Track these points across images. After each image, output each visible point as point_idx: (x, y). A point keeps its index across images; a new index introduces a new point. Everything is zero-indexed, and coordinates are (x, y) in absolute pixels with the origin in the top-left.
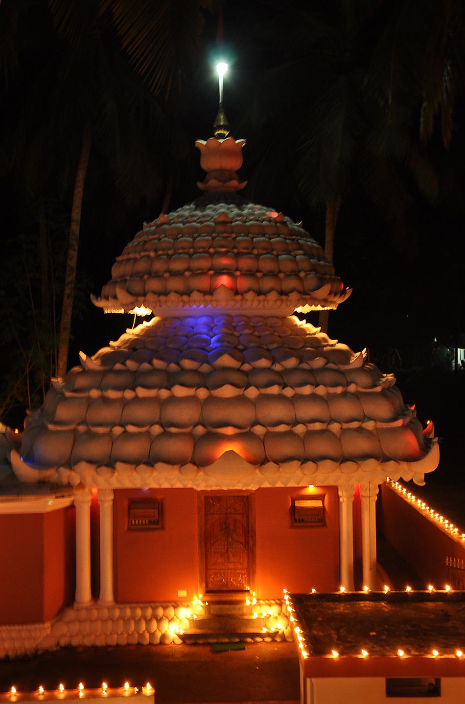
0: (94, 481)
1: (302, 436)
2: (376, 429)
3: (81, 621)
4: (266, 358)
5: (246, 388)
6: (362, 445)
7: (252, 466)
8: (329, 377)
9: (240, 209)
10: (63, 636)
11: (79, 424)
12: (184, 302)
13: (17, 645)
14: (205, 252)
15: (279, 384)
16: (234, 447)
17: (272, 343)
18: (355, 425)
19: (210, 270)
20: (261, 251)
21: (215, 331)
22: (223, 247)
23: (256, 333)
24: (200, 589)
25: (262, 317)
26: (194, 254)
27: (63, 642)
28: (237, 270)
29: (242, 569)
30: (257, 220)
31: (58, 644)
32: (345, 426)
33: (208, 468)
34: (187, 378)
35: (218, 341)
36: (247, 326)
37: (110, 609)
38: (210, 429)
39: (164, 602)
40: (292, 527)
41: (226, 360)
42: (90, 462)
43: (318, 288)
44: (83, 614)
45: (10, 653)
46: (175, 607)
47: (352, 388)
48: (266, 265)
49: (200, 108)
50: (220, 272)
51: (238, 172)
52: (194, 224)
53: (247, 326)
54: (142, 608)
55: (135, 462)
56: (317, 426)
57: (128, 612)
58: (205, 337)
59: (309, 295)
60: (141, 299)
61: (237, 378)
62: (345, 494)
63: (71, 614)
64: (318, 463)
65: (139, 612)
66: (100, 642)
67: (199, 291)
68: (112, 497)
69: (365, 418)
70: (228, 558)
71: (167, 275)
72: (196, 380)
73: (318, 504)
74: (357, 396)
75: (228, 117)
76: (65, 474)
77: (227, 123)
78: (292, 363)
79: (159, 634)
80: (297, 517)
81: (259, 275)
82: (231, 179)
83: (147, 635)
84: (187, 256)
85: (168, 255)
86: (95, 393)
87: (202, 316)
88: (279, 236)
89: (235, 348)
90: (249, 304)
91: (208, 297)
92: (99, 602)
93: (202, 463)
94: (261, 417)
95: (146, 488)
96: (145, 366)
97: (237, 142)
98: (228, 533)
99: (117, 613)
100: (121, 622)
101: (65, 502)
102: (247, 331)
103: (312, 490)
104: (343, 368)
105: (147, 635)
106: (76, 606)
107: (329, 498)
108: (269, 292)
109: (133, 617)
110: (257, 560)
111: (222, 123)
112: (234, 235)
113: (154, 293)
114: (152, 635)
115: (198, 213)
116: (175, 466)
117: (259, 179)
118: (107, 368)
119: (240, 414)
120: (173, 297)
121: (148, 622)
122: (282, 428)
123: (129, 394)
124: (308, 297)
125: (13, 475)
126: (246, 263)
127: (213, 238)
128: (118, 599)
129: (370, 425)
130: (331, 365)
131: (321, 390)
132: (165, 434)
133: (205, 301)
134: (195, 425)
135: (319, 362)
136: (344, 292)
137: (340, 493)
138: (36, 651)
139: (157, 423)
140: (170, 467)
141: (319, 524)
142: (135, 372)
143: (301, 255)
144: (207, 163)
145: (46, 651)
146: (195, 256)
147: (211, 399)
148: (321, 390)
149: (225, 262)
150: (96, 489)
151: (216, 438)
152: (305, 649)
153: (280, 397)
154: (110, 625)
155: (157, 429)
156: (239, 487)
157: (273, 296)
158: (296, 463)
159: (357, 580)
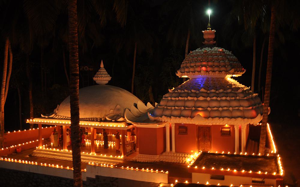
1: (221, 111)
4: (222, 89)
6: (238, 114)
7: (205, 119)
8: (231, 95)
12: (194, 74)
13: (150, 159)
14: (200, 61)
15: (216, 97)
16: (201, 114)
17: (218, 85)
18: (237, 108)
19: (201, 65)
20: (215, 60)
21: (203, 82)
22: (204, 59)
23: (214, 83)
24: (197, 151)
27: (161, 160)
28: (214, 65)
29: (208, 146)
30: (215, 52)
32: (234, 108)
33: (193, 119)
34: (192, 95)
35: (203, 85)
36: (212, 80)
37: (174, 153)
40: (221, 136)
41: (203, 90)
42: (166, 116)
43: (230, 70)
44: (172, 154)
47: (238, 98)
48: (216, 64)
49: (204, 22)
50: (203, 66)
51: (214, 39)
52: (198, 53)
53: (212, 80)
54: (182, 154)
55: (175, 116)
56: (225, 108)
57: (178, 155)
58: (200, 83)
60: (183, 74)
61: (204, 95)
63: (164, 154)
65: (181, 155)
66: (170, 161)
67: (197, 71)
68: (174, 125)
69: (240, 106)
70: (205, 143)
71: (190, 67)
72: (194, 95)
73: (229, 130)
74: (239, 100)
77: (211, 26)
78: (221, 91)
79: (184, 161)
81: (214, 67)
82: (211, 40)
86: (169, 98)
87: (201, 78)
90: (211, 75)
91: (199, 73)
92: (172, 152)
93: (192, 117)
94: (210, 105)
95: (183, 123)
96: (183, 91)
97: (212, 31)
101: (162, 126)
102: (211, 82)
103: (227, 126)
104: (236, 92)
105: (181, 161)
106: (166, 152)
109: (179, 156)
111: (209, 26)
112: (208, 56)
113: (186, 72)
114: (183, 161)
115: (200, 50)
116: (185, 118)
117: (219, 41)
118: (174, 92)
119: (204, 105)
121: (182, 158)
122: (215, 109)
123: (177, 99)
124: (227, 72)
125: (149, 119)
126: (210, 64)
127: (202, 57)
128: (177, 151)
129: (241, 108)
130: (233, 91)
131: (228, 98)
132: (185, 109)
133: (219, 73)
135: (229, 91)
136: (243, 71)
137: (235, 127)
139: (183, 106)
140: (184, 118)
141: (229, 135)
142: (180, 93)
144: (205, 37)
145: (156, 162)
147: (198, 100)
149: (204, 63)
151: (196, 110)
152: (282, 169)
155: (183, 108)
156: (207, 124)
157: (217, 72)
158: (217, 118)
159: (240, 150)
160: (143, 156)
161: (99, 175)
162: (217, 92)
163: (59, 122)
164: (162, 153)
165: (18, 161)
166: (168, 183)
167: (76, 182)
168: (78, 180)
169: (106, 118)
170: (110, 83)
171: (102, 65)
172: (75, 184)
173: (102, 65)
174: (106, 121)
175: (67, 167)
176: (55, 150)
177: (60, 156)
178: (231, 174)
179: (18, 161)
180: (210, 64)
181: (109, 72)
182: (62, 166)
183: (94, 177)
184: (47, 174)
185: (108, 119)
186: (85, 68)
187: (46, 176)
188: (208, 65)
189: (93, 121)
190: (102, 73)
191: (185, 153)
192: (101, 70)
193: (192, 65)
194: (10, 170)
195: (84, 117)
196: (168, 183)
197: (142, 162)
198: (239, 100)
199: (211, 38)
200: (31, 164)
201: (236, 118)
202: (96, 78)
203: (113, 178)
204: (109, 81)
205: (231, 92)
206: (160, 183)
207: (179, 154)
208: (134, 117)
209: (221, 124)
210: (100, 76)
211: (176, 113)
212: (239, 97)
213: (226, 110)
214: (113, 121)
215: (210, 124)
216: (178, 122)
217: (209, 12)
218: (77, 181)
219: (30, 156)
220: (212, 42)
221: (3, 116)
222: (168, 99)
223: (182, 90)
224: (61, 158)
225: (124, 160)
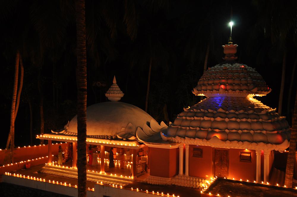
0: (184, 142)
2: (267, 133)
3: (179, 179)
5: (225, 118)
6: (260, 138)
7: (221, 141)
9: (232, 65)
10: (174, 182)
11: (179, 126)
13: (162, 182)
16: (218, 136)
18: (259, 131)
24: (212, 176)
25: (238, 97)
26: (235, 79)
27: (173, 184)
31: (172, 184)
32: (255, 132)
34: (209, 115)
38: (213, 130)
39: (202, 178)
41: (220, 110)
42: (179, 136)
44: (180, 177)
45: (160, 184)
46: (205, 180)
47: (260, 120)
48: (237, 82)
50: (222, 84)
55: (190, 137)
56: (246, 131)
59: (250, 91)
60: (200, 92)
61: (223, 115)
62: (258, 153)
63: (177, 177)
64: (244, 142)
65: (194, 179)
67: (215, 90)
68: (189, 147)
70: (221, 168)
73: (249, 155)
74: (262, 123)
75: (232, 38)
76: (173, 139)
79: (198, 186)
80: (241, 158)
83: (195, 186)
84: (213, 79)
85: (209, 79)
86: (184, 118)
88: (243, 73)
89: (234, 107)
91: (217, 91)
92: (185, 175)
93: (208, 139)
94: (228, 127)
99: (189, 178)
100: (192, 181)
103: (247, 150)
107: (252, 154)
108: (236, 90)
109: (192, 181)
111: (231, 40)
113: (203, 90)
117: (240, 57)
120: (208, 91)
121: (196, 182)
122: (234, 131)
123: (192, 118)
124: (249, 91)
126: (230, 81)
129: (264, 132)
130: (255, 113)
131: (249, 120)
132: (200, 130)
134: (209, 128)
135: (251, 112)
136: (268, 91)
137: (256, 153)
138: (166, 184)
139: (198, 127)
140: (199, 139)
142: (196, 112)
143: (249, 78)
144: (225, 52)
146: (215, 79)
148: (249, 120)
149: (223, 81)
150: (183, 144)
151: (213, 132)
153: (236, 122)
155: (198, 129)
157: (237, 91)
161: (107, 195)
164: (174, 176)
165: (27, 177)
169: (117, 137)
170: (123, 100)
171: (115, 81)
173: (115, 81)
174: (116, 139)
179: (64, 184)
185: (119, 137)
189: (104, 139)
190: (114, 89)
192: (114, 86)
193: (210, 82)
198: (262, 123)
204: (122, 98)
210: (112, 92)
211: (190, 134)
216: (193, 144)
224: (70, 176)
225: (134, 181)
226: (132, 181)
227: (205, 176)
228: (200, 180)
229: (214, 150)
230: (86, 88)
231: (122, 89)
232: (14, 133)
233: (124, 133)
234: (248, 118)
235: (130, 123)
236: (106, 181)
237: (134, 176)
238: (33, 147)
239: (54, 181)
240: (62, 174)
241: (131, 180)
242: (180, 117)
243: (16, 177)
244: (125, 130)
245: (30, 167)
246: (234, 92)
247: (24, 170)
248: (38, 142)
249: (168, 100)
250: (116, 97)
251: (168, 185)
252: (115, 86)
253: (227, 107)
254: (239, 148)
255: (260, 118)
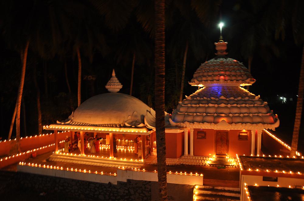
6: (258, 120)
8: (241, 102)
10: (181, 162)
11: (186, 113)
18: (256, 114)
32: (254, 115)
33: (217, 124)
34: (212, 102)
41: (222, 97)
45: (169, 164)
47: (256, 105)
48: (233, 73)
49: (216, 35)
56: (246, 114)
60: (201, 82)
61: (225, 102)
63: (183, 157)
65: (199, 158)
68: (193, 130)
70: (222, 147)
71: (207, 76)
72: (215, 102)
73: (246, 134)
74: (257, 107)
76: (182, 125)
78: (240, 98)
82: (224, 52)
86: (189, 105)
93: (216, 123)
98: (222, 140)
99: (194, 158)
103: (244, 131)
104: (253, 100)
106: (184, 155)
109: (198, 159)
110: (229, 147)
117: (230, 52)
121: (202, 160)
122: (237, 115)
123: (198, 106)
126: (228, 73)
129: (260, 115)
130: (250, 99)
131: (247, 105)
132: (207, 115)
136: (254, 80)
137: (252, 132)
144: (217, 48)
147: (219, 107)
148: (247, 105)
149: (222, 73)
151: (219, 117)
154: (192, 160)
155: (205, 114)
157: (235, 81)
159: (256, 153)
160: (174, 160)
161: (131, 178)
162: (236, 99)
163: (74, 128)
164: (181, 156)
165: (83, 171)
166: (203, 185)
167: (162, 191)
168: (164, 188)
169: (125, 124)
170: (121, 91)
171: (114, 74)
172: (161, 192)
173: (114, 74)
174: (125, 127)
175: (114, 173)
176: (126, 160)
177: (78, 160)
178: (282, 175)
179: (83, 171)
180: (228, 73)
181: (121, 81)
182: (90, 171)
183: (126, 181)
184: (74, 178)
185: (127, 125)
186: (90, 77)
187: (73, 180)
188: (237, 75)
189: (113, 127)
191: (203, 156)
192: (113, 79)
193: (210, 74)
194: (35, 175)
195: (102, 124)
196: (203, 185)
197: (170, 165)
198: (257, 107)
199: (223, 50)
200: (56, 169)
201: (258, 124)
202: (109, 86)
203: (146, 181)
204: (121, 90)
205: (240, 100)
206: (195, 185)
207: (203, 157)
208: (152, 123)
209: (239, 129)
210: (113, 84)
211: (198, 119)
212: (257, 104)
213: (247, 116)
214: (133, 126)
215: (229, 130)
216: (197, 128)
217: (221, 25)
218: (163, 189)
219: (47, 160)
220: (225, 53)
221: (19, 123)
222: (185, 105)
223: (201, 98)
224: (79, 162)
225: (145, 163)
226: (143, 164)
227: (209, 154)
228: (205, 158)
229: (216, 132)
230: (164, 74)
231: (120, 81)
232: (19, 125)
233: (131, 121)
234: (246, 104)
235: (135, 112)
236: (114, 165)
237: (144, 159)
238: (34, 137)
239: (80, 170)
240: (71, 161)
241: (142, 163)
242: (184, 105)
243: (31, 166)
244: (131, 118)
245: (37, 156)
246: (232, 81)
247: (31, 158)
248: (45, 132)
249: (164, 91)
250: (116, 88)
251: (177, 165)
252: (114, 79)
253: (226, 95)
254: (238, 129)
255: (255, 104)
